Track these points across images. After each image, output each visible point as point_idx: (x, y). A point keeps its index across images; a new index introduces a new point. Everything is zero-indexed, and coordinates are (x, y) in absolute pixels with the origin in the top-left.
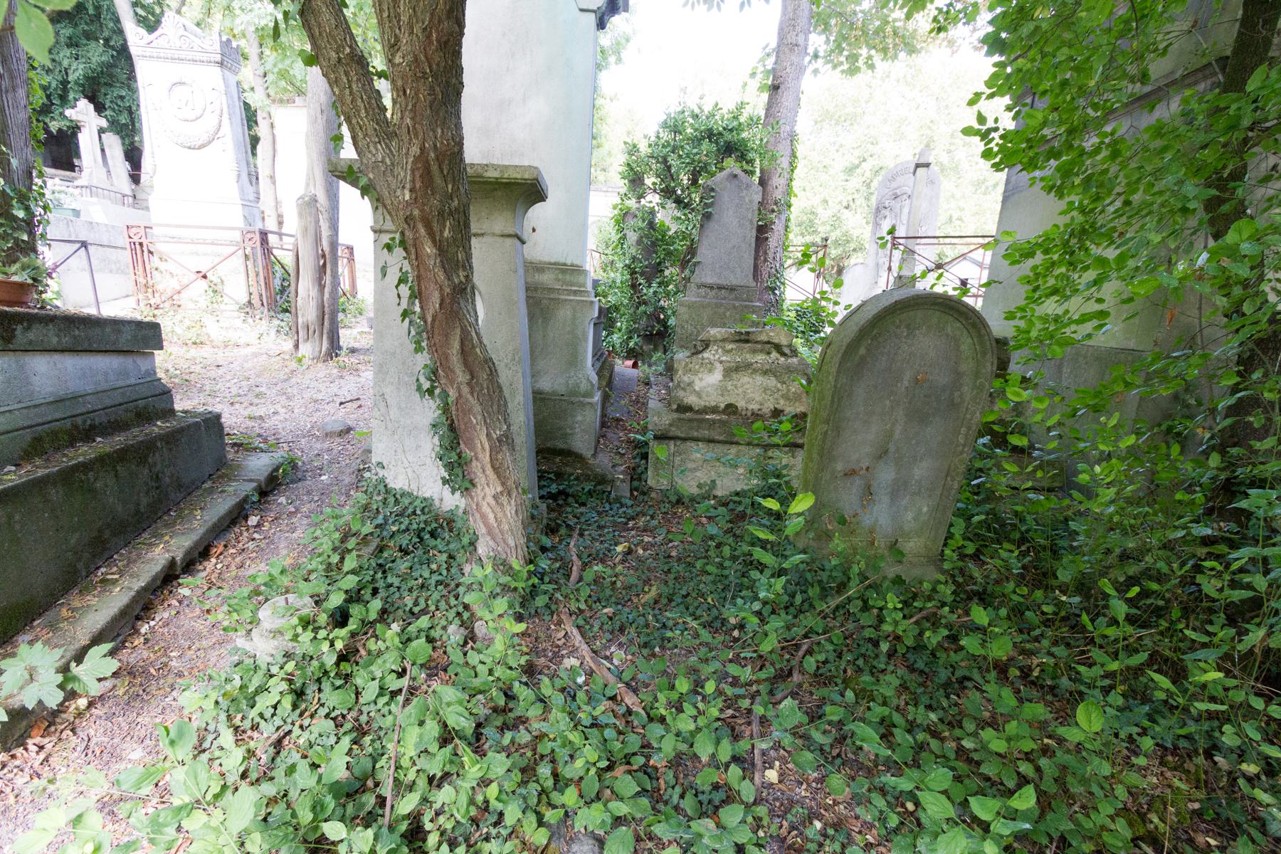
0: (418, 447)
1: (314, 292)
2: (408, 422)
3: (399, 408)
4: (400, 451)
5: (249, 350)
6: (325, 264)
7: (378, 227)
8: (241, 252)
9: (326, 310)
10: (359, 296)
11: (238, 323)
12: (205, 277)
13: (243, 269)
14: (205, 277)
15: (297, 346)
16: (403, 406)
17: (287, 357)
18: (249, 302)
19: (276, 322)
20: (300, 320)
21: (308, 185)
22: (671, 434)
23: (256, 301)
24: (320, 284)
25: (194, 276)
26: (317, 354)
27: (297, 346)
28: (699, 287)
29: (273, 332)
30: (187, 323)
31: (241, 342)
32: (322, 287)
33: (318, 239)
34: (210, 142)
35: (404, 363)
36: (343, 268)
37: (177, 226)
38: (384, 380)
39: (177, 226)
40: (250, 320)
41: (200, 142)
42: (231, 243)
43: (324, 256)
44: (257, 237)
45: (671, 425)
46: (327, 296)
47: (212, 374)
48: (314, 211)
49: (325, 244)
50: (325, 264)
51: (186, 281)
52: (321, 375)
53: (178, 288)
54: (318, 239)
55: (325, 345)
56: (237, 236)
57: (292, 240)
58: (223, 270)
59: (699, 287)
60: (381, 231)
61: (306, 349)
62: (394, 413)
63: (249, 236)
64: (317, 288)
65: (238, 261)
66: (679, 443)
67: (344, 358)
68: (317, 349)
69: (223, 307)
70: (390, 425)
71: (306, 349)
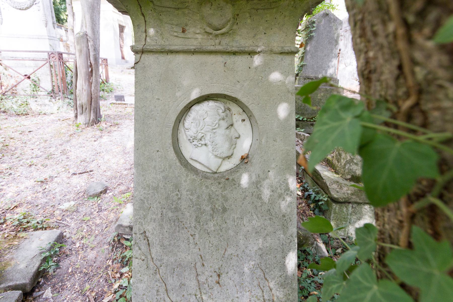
0: (182, 285)
1: (86, 87)
2: (172, 260)
3: (162, 246)
4: (162, 290)
5: (52, 117)
6: (92, 71)
7: (140, 47)
8: (48, 64)
9: (93, 96)
10: (111, 81)
11: (47, 101)
12: (29, 78)
13: (49, 72)
14: (29, 78)
15: (76, 117)
16: (166, 243)
17: (71, 123)
18: (53, 90)
19: (67, 100)
20: (78, 103)
21: (82, 26)
22: (352, 200)
23: (56, 90)
24: (89, 82)
25: (23, 78)
26: (87, 121)
27: (76, 117)
28: (305, 79)
29: (65, 106)
30: (20, 102)
31: (49, 112)
32: (90, 84)
33: (88, 56)
34: (31, 6)
35: (167, 198)
36: (102, 70)
37: (13, 51)
38: (145, 217)
39: (13, 51)
40: (53, 100)
41: (26, 6)
42: (43, 60)
43: (91, 66)
44: (57, 57)
45: (352, 194)
46: (93, 88)
47: (25, 138)
48: (85, 40)
49: (92, 59)
50: (92, 71)
51: (19, 80)
52: (90, 135)
53: (15, 84)
54: (88, 56)
55: (92, 117)
56: (46, 56)
57: (73, 56)
58: (39, 73)
59: (305, 79)
60: (143, 52)
61: (82, 119)
62: (156, 251)
63: (52, 56)
64: (87, 83)
65: (46, 69)
66: (355, 206)
67: (103, 125)
68: (88, 119)
69: (39, 93)
70: (151, 265)
71: (82, 119)
